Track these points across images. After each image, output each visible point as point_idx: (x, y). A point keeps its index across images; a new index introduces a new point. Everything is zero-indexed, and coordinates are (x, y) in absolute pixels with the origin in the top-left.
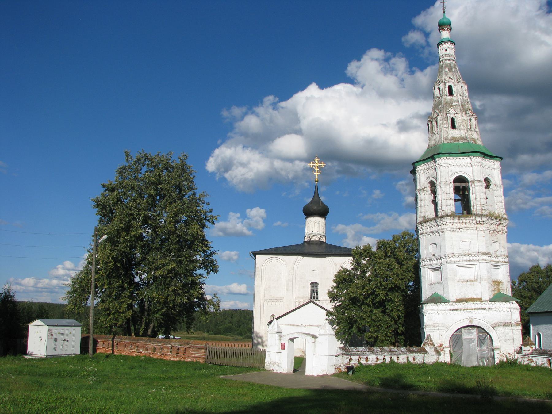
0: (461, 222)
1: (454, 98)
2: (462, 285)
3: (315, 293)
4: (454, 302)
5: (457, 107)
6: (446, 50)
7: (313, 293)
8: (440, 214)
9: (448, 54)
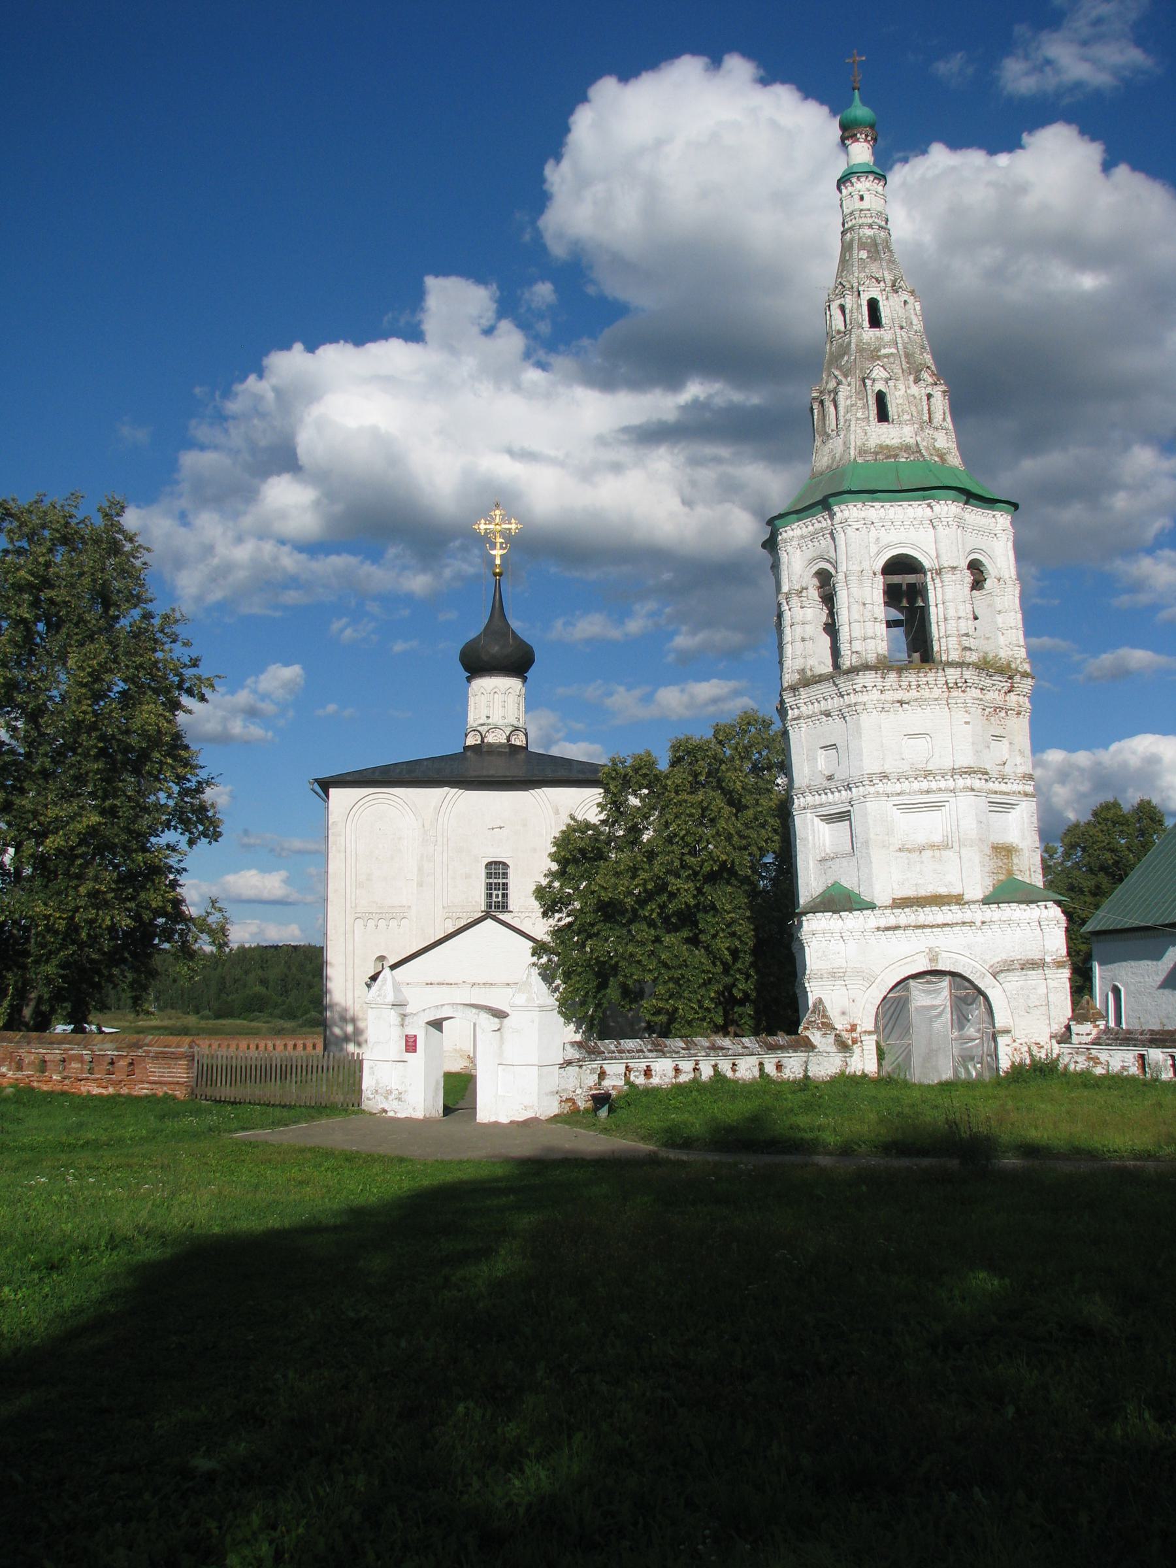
0: (904, 684)
1: (885, 334)
2: (908, 858)
3: (500, 893)
4: (886, 907)
5: (892, 360)
6: (862, 198)
7: (495, 893)
8: (846, 663)
9: (869, 210)
